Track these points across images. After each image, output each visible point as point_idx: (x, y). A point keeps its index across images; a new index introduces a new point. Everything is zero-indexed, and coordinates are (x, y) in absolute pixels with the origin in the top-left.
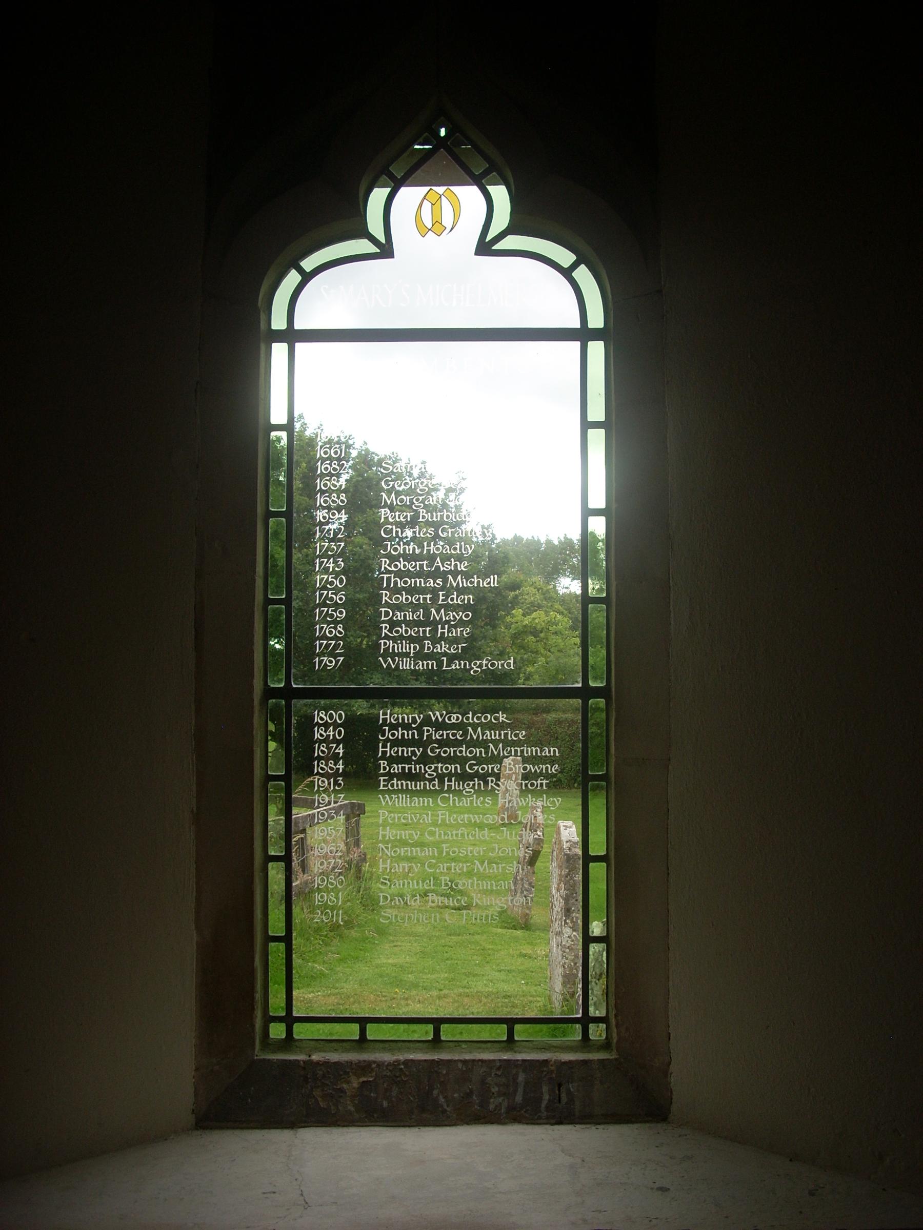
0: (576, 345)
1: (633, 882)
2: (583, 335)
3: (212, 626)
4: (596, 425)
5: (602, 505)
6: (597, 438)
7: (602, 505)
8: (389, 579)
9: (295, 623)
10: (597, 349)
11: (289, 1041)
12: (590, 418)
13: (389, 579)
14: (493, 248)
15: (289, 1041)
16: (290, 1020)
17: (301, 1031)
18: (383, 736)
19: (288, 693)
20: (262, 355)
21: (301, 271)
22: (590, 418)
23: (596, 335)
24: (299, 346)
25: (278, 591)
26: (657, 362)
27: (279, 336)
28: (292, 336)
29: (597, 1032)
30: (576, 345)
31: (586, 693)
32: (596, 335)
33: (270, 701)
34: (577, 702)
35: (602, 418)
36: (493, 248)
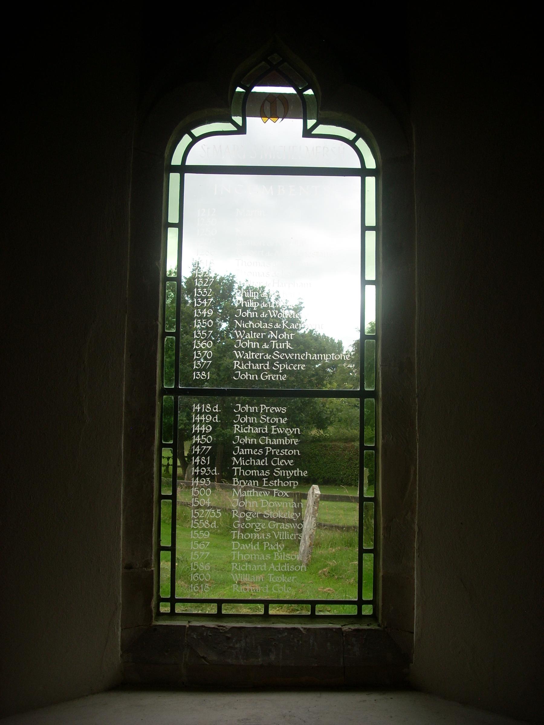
0: (359, 179)
1: (388, 539)
2: (363, 172)
3: (125, 362)
4: (371, 228)
5: (373, 224)
6: (371, 236)
7: (373, 224)
8: (238, 470)
9: (182, 353)
10: (371, 181)
11: (172, 614)
12: (367, 224)
13: (238, 470)
14: (313, 133)
15: (172, 614)
16: (173, 601)
17: (179, 608)
18: (235, 453)
19: (176, 392)
20: (165, 179)
21: (192, 135)
22: (367, 224)
23: (370, 172)
24: (187, 175)
25: (171, 327)
26: (406, 230)
27: (176, 169)
28: (183, 169)
29: (367, 610)
30: (359, 179)
31: (362, 395)
32: (370, 172)
33: (164, 396)
34: (355, 401)
35: (374, 278)
36: (313, 133)
